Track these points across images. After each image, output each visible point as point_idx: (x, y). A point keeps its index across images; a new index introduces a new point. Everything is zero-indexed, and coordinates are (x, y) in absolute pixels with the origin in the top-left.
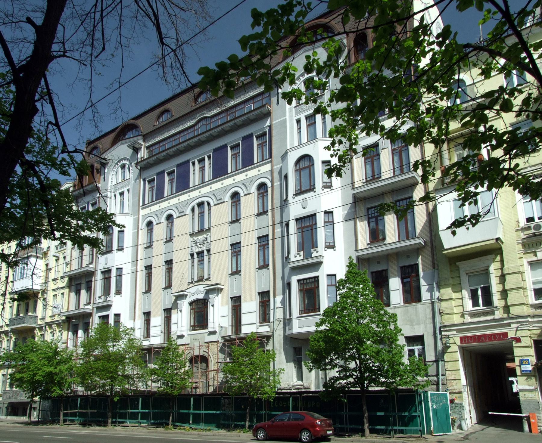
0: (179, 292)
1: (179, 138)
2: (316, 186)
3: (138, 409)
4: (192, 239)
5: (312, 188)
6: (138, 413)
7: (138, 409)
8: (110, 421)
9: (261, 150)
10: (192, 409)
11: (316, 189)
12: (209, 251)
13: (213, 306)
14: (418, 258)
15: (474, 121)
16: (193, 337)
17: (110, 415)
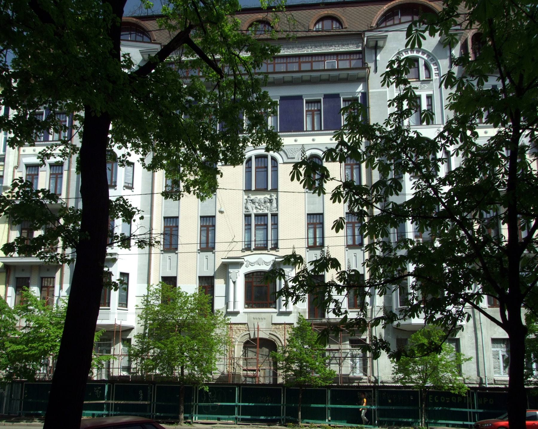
0: (228, 258)
1: (311, 62)
2: (118, 184)
3: (235, 402)
4: (246, 197)
5: (113, 184)
6: (234, 406)
7: (235, 402)
8: (182, 416)
9: (311, 116)
10: (364, 404)
11: (117, 187)
12: (275, 216)
13: (234, 283)
14: (56, 272)
15: (350, 152)
16: (252, 316)
17: (182, 408)
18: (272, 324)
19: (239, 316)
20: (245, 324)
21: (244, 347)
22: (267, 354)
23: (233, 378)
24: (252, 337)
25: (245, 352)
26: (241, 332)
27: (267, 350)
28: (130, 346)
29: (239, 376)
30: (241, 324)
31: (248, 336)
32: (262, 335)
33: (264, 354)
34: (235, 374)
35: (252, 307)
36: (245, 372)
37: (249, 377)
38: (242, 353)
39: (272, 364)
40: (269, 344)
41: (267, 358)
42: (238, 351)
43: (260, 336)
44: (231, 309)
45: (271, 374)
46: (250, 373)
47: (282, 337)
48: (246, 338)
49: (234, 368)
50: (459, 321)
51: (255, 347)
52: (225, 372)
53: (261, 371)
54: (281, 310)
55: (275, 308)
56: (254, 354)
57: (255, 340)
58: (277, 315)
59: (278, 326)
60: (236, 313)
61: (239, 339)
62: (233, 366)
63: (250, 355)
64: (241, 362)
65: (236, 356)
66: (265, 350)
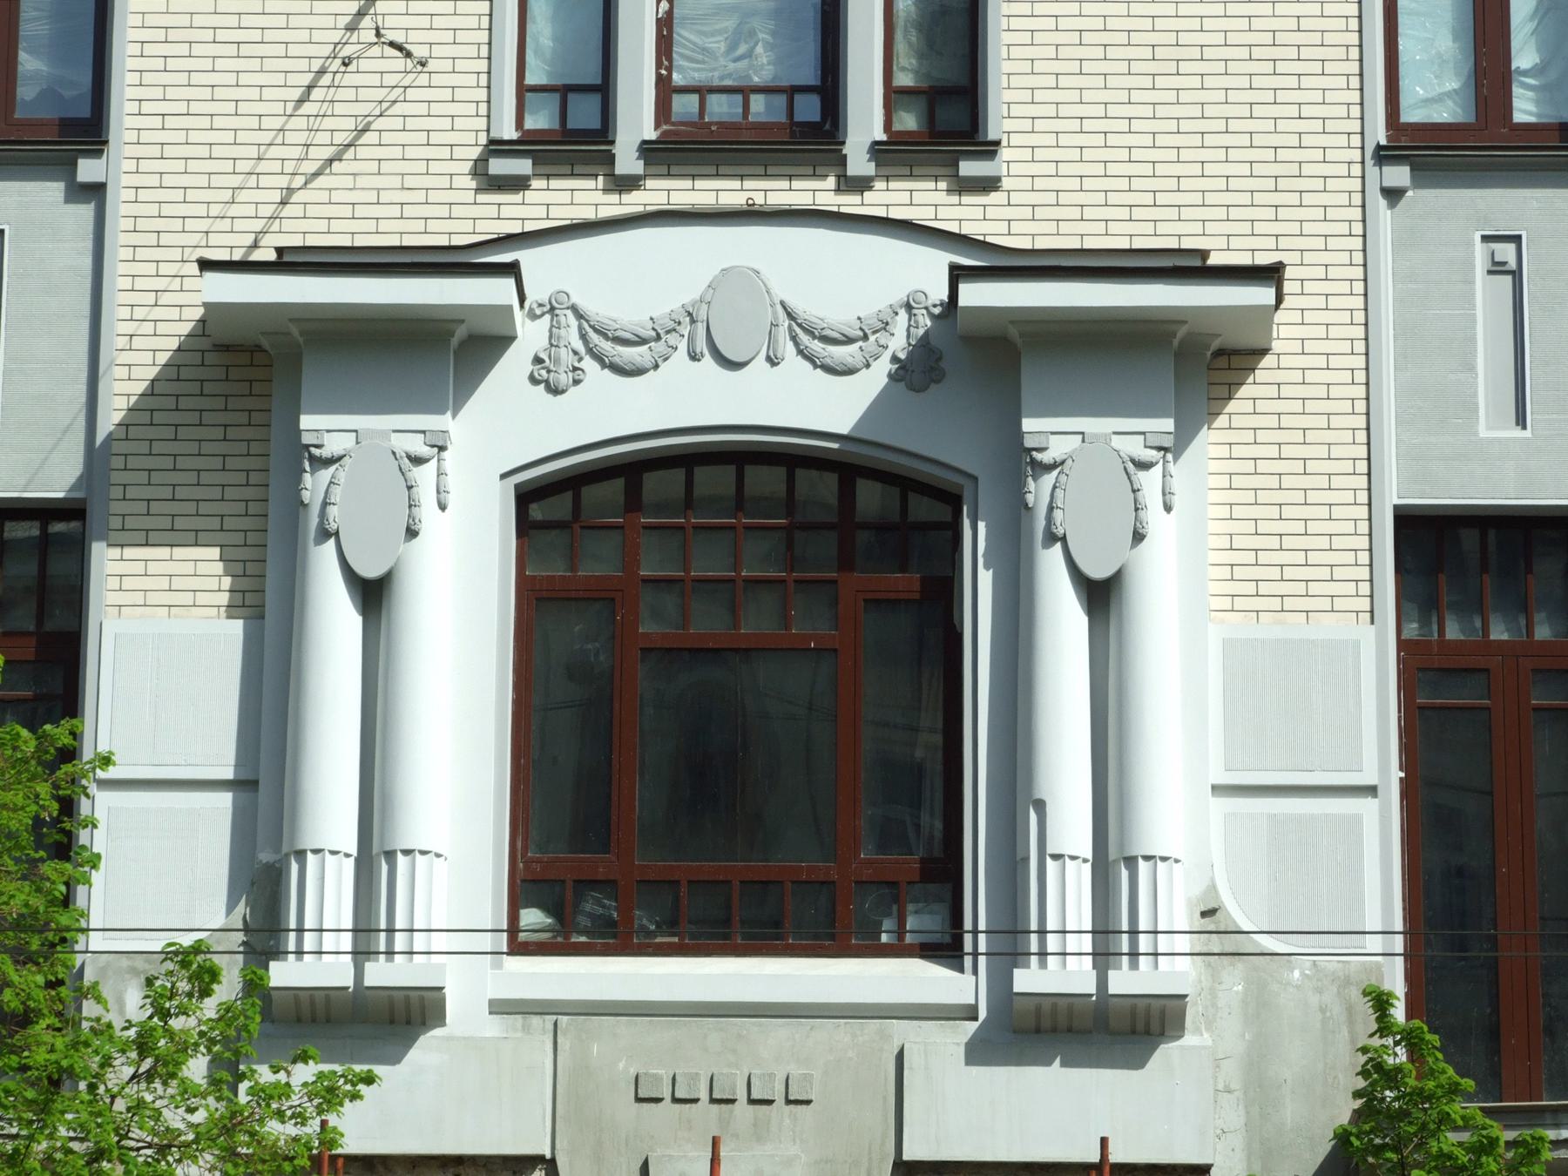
16: (619, 1053)
19: (426, 1051)
35: (617, 939)
44: (317, 965)
54: (1027, 980)
58: (978, 1053)
60: (404, 1017)
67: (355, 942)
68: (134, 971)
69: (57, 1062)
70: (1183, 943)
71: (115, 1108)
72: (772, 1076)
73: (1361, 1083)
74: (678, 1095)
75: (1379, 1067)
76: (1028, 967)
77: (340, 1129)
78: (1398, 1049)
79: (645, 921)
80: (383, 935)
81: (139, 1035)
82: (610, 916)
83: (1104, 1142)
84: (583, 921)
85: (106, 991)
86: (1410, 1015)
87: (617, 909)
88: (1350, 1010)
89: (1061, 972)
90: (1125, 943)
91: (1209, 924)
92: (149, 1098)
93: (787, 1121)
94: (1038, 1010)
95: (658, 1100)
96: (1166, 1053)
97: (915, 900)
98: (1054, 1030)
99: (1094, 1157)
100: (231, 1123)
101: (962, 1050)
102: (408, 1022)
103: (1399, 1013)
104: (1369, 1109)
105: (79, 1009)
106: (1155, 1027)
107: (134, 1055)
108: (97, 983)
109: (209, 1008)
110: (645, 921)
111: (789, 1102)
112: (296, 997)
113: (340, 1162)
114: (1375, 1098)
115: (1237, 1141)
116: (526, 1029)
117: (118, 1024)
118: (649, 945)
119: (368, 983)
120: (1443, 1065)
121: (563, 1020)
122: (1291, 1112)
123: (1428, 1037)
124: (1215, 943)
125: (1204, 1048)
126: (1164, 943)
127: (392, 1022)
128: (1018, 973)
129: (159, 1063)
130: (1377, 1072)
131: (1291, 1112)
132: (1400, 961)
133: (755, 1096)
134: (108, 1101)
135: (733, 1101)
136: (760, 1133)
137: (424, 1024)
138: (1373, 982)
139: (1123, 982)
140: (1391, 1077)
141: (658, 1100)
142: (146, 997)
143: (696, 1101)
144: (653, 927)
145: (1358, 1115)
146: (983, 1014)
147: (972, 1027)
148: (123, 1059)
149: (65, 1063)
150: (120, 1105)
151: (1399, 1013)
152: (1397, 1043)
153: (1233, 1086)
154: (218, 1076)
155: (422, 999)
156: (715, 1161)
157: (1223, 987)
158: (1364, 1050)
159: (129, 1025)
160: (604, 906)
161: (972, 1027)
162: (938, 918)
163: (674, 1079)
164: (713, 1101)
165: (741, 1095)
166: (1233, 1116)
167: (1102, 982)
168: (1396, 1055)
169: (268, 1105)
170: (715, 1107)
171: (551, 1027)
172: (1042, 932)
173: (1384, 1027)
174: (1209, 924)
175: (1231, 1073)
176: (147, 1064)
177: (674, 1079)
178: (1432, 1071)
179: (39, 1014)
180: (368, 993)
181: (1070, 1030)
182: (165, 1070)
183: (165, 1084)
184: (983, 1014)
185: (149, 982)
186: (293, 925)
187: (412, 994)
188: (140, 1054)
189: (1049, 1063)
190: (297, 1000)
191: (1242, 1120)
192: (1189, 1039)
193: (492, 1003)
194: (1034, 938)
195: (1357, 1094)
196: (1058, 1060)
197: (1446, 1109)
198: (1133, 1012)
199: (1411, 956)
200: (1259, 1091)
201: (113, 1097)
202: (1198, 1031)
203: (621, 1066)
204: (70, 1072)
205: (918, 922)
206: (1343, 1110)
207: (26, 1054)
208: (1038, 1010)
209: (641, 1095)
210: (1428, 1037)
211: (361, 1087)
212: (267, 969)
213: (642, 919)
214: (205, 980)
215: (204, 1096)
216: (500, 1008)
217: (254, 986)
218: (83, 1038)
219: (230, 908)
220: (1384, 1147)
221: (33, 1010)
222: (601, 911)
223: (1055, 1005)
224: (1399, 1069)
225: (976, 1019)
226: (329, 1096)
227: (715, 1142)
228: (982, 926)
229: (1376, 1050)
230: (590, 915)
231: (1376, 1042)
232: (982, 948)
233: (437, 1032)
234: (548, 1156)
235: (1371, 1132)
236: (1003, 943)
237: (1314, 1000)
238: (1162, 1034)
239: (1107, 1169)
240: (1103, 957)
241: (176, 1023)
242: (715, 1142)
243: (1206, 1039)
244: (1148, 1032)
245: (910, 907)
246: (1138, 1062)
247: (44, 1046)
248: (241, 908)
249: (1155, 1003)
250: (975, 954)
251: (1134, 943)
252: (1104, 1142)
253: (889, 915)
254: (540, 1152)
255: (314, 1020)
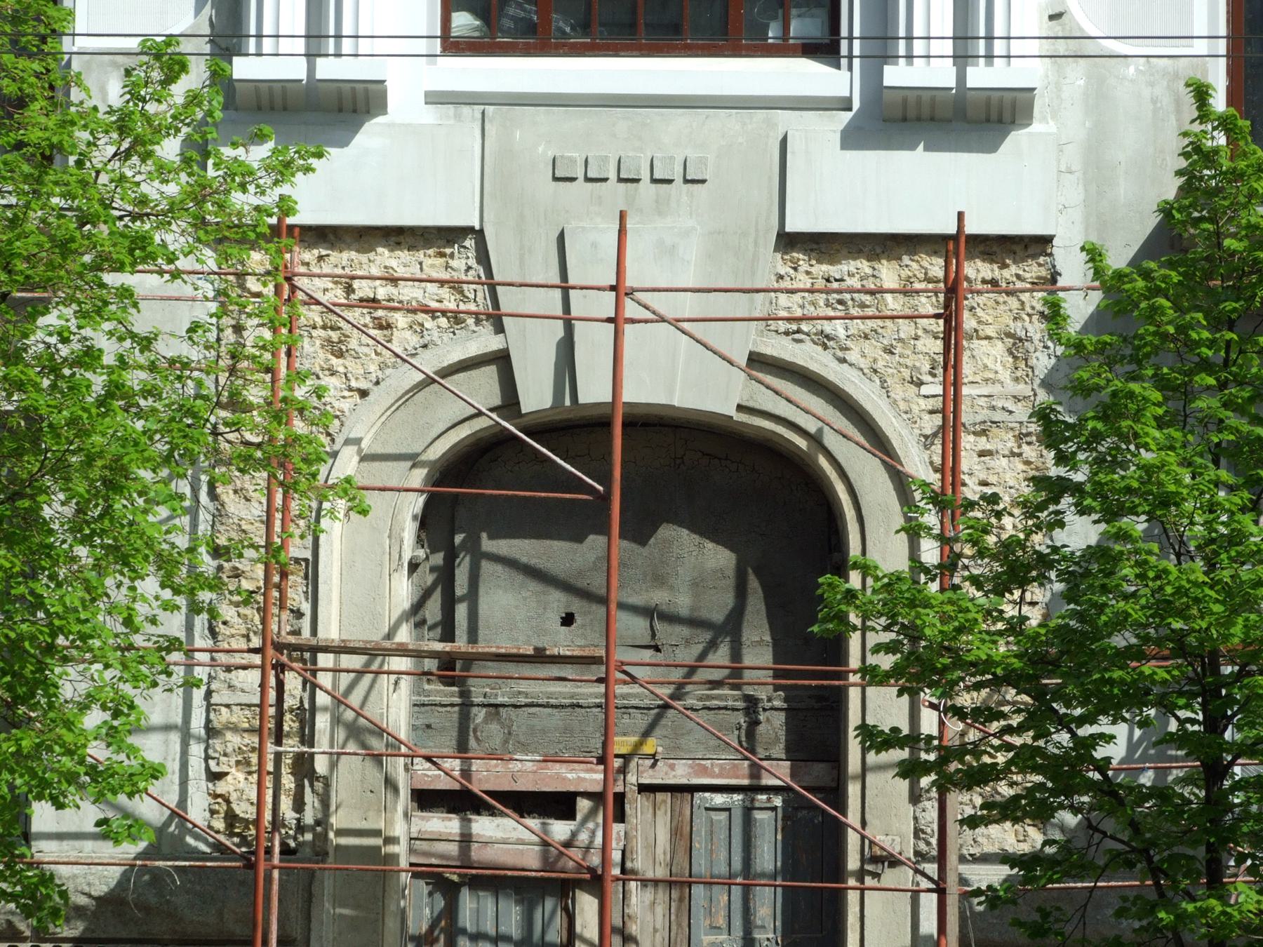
16: (540, 138)
18: (789, 242)
19: (371, 135)
20: (444, 237)
21: (438, 522)
22: (718, 606)
23: (303, 892)
24: (536, 395)
25: (446, 576)
26: (404, 338)
27: (719, 558)
28: (1154, 404)
29: (371, 868)
30: (397, 236)
31: (482, 389)
32: (678, 374)
33: (682, 603)
34: (320, 850)
35: (536, 39)
36: (444, 824)
37: (497, 881)
38: (403, 591)
39: (774, 724)
40: (754, 494)
41: (721, 656)
42: (364, 571)
43: (648, 387)
44: (271, 62)
45: (767, 856)
46: (505, 838)
47: (944, 437)
48: (445, 424)
49: (303, 766)
50: (45, 506)
51: (580, 520)
52: (197, 811)
53: (637, 807)
54: (895, 75)
55: (825, 49)
56: (558, 601)
57: (578, 429)
58: (853, 138)
59: (852, 270)
60: (352, 106)
61: (386, 410)
62: (291, 746)
63: (509, 612)
64: (394, 705)
65: (330, 631)
66: (696, 565)
67: (308, 46)
68: (115, 65)
69: (48, 139)
70: (1034, 47)
71: (100, 181)
72: (672, 158)
73: (1183, 163)
74: (590, 175)
75: (1198, 149)
76: (897, 64)
77: (294, 197)
78: (1215, 133)
79: (561, 24)
80: (332, 40)
81: (119, 120)
82: (531, 19)
83: (961, 215)
84: (507, 23)
85: (89, 81)
86: (1230, 102)
87: (536, 13)
88: (1178, 102)
89: (925, 70)
90: (981, 47)
91: (1056, 28)
92: (129, 173)
93: (685, 198)
94: (905, 101)
95: (572, 179)
96: (1017, 139)
97: (798, 6)
98: (919, 119)
99: (952, 229)
100: (200, 193)
101: (839, 135)
102: (355, 111)
103: (1219, 103)
104: (1190, 184)
105: (68, 94)
106: (1007, 116)
107: (115, 136)
108: (80, 73)
109: (179, 90)
110: (561, 24)
111: (686, 181)
112: (257, 89)
113: (297, 231)
114: (1195, 177)
115: (1077, 214)
116: (458, 117)
117: (103, 108)
118: (564, 45)
119: (318, 76)
120: (1254, 147)
121: (490, 110)
122: (1124, 190)
123: (1240, 122)
124: (1061, 47)
125: (1049, 134)
126: (1017, 47)
127: (340, 110)
128: (888, 69)
129: (133, 133)
130: (1198, 154)
131: (1124, 190)
132: (1223, 61)
133: (656, 176)
134: (94, 175)
135: (637, 181)
136: (660, 208)
137: (368, 112)
138: (1199, 77)
139: (980, 77)
140: (1209, 157)
141: (572, 179)
142: (125, 86)
143: (606, 180)
144: (568, 30)
145: (1184, 190)
146: (856, 105)
147: (847, 116)
148: (106, 139)
149: (55, 140)
150: (104, 178)
151: (1219, 103)
152: (1214, 129)
153: (1073, 169)
154: (188, 155)
155: (366, 90)
156: (622, 232)
157: (1068, 81)
158: (1185, 134)
159: (111, 112)
160: (524, 10)
161: (847, 116)
162: (818, 21)
163: (586, 161)
164: (620, 180)
165: (645, 175)
166: (1074, 193)
167: (961, 77)
168: (1213, 138)
169: (233, 180)
170: (622, 185)
171: (480, 116)
172: (909, 38)
173: (1203, 111)
174: (1056, 28)
175: (1073, 156)
176: (125, 145)
177: (586, 161)
178: (1245, 154)
179: (33, 98)
180: (320, 84)
181: (932, 119)
182: (139, 148)
183: (143, 161)
184: (856, 105)
185: (128, 73)
186: (253, 31)
187: (357, 86)
188: (120, 135)
189: (913, 147)
190: (257, 90)
191: (1082, 197)
192: (1036, 127)
193: (427, 94)
194: (902, 43)
195: (1179, 173)
196: (922, 145)
197: (1255, 185)
198: (988, 102)
199: (1233, 56)
200: (1096, 168)
201: (98, 173)
202: (1044, 120)
203: (540, 149)
204: (59, 147)
205: (802, 26)
206: (1170, 188)
207: (22, 132)
208: (905, 101)
209: (558, 175)
210: (1240, 122)
211: (311, 160)
212: (230, 63)
213: (559, 22)
214: (174, 67)
215: (177, 171)
216: (435, 98)
217: (220, 79)
218: (69, 118)
219: (198, 10)
220: (1201, 219)
221: (28, 96)
222: (523, 14)
223: (919, 97)
224: (1216, 151)
225: (850, 109)
226: (283, 170)
227: (622, 216)
228: (856, 33)
229: (1196, 135)
230: (513, 18)
231: (1197, 127)
232: (856, 51)
233: (380, 119)
234: (477, 227)
235: (1190, 206)
236: (875, 48)
237: (1146, 92)
238: (1013, 122)
239: (963, 239)
240: (962, 58)
241: (151, 108)
242: (622, 216)
243: (1051, 127)
244: (1000, 121)
245: (794, 12)
246: (991, 147)
247: (38, 124)
248: (208, 10)
249: (1007, 95)
250: (850, 57)
251: (989, 47)
252: (961, 215)
253: (775, 18)
254: (471, 224)
255: (272, 109)
